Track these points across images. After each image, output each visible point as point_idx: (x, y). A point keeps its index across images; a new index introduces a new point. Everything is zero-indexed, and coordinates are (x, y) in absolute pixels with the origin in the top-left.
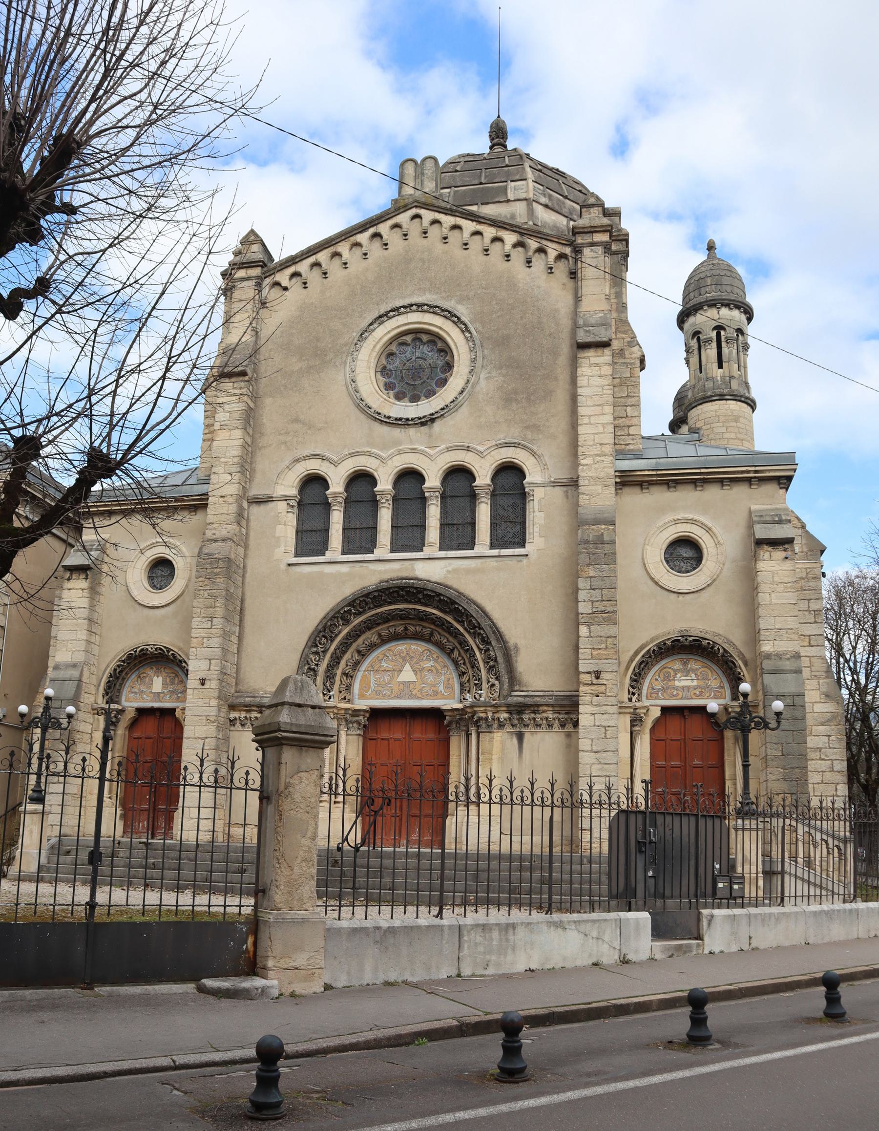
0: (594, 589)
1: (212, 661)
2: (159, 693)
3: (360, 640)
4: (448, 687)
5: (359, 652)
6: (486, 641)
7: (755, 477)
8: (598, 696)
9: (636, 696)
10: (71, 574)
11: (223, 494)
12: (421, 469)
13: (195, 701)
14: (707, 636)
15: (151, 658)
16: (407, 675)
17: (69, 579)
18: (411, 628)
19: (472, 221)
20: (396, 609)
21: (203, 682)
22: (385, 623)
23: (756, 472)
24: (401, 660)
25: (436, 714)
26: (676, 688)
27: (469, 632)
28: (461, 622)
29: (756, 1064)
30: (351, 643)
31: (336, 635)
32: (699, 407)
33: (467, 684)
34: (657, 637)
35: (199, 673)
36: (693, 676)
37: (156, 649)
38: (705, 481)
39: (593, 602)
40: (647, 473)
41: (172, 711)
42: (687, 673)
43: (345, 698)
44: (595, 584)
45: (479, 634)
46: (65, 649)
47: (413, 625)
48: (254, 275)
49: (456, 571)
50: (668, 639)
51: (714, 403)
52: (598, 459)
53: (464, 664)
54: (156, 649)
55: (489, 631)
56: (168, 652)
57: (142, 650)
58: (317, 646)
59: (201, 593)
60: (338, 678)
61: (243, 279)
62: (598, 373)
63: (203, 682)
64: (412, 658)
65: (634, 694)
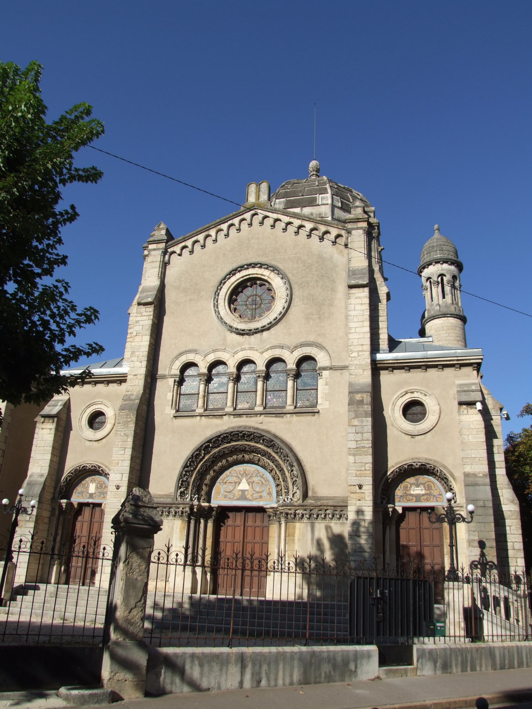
0: (357, 433)
1: (124, 475)
2: (93, 494)
7: (457, 364)
8: (359, 500)
9: (386, 500)
10: (45, 420)
11: (136, 374)
12: (298, 359)
13: (112, 499)
14: (430, 462)
15: (89, 472)
16: (244, 485)
17: (43, 423)
19: (287, 216)
20: (237, 445)
21: (118, 487)
23: (458, 360)
24: (240, 476)
25: (261, 510)
26: (412, 495)
32: (432, 322)
33: (280, 492)
34: (399, 463)
35: (115, 482)
36: (422, 487)
37: (92, 467)
38: (445, 366)
39: (357, 441)
40: (391, 362)
41: (100, 505)
42: (418, 486)
44: (359, 429)
45: (288, 461)
46: (37, 465)
48: (161, 247)
50: (405, 465)
51: (440, 319)
52: (360, 353)
53: (279, 479)
54: (92, 467)
56: (99, 468)
57: (84, 467)
59: (120, 432)
61: (155, 250)
62: (360, 302)
63: (118, 487)
65: (384, 499)
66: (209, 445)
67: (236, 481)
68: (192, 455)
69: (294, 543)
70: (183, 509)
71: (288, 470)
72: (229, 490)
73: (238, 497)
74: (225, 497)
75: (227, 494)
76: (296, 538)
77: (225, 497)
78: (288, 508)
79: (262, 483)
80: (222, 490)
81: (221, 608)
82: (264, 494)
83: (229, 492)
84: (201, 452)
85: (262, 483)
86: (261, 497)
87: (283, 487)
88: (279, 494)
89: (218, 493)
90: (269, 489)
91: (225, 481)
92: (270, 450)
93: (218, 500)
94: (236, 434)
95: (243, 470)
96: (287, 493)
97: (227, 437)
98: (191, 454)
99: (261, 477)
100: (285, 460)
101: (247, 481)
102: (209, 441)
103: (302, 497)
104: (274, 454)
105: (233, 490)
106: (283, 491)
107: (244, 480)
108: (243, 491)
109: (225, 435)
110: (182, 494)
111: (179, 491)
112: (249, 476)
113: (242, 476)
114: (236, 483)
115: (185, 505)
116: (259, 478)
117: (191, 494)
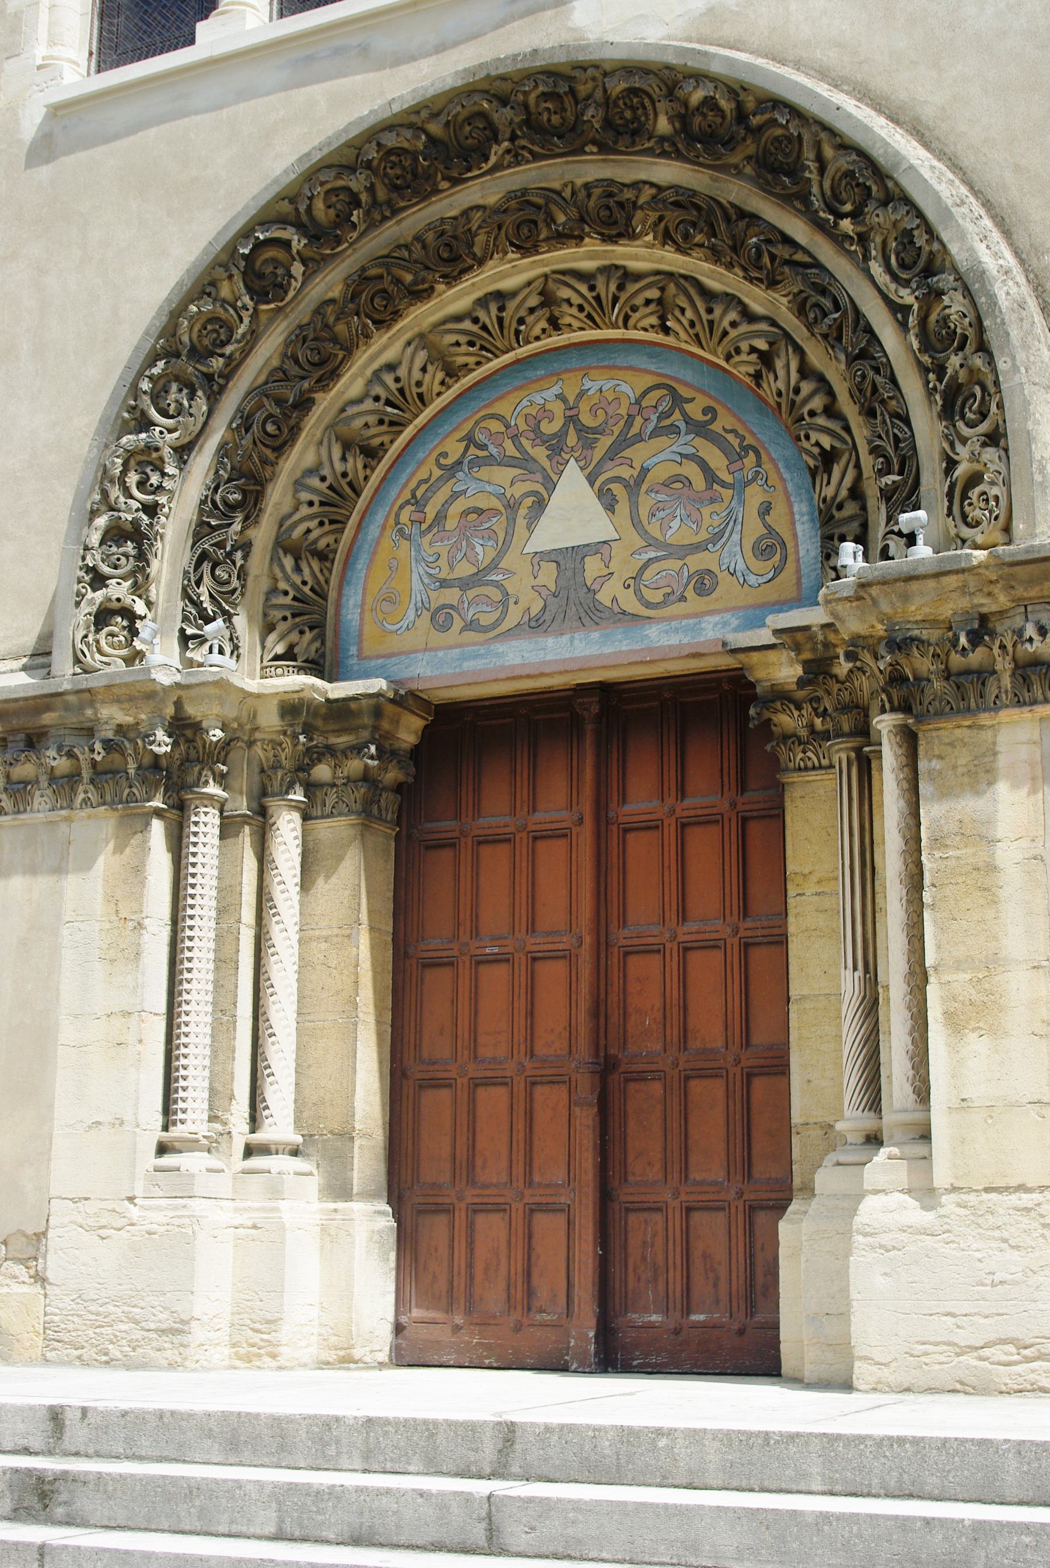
24: (540, 453)
27: (839, 240)
58: (145, 424)
64: (588, 436)
69: (989, 894)
71: (898, 311)
72: (465, 570)
73: (536, 609)
74: (441, 618)
75: (452, 596)
77: (441, 618)
79: (710, 476)
85: (710, 476)
86: (704, 583)
87: (867, 461)
90: (766, 509)
95: (558, 408)
99: (700, 429)
101: (591, 480)
108: (570, 559)
112: (605, 442)
113: (556, 446)
114: (512, 506)
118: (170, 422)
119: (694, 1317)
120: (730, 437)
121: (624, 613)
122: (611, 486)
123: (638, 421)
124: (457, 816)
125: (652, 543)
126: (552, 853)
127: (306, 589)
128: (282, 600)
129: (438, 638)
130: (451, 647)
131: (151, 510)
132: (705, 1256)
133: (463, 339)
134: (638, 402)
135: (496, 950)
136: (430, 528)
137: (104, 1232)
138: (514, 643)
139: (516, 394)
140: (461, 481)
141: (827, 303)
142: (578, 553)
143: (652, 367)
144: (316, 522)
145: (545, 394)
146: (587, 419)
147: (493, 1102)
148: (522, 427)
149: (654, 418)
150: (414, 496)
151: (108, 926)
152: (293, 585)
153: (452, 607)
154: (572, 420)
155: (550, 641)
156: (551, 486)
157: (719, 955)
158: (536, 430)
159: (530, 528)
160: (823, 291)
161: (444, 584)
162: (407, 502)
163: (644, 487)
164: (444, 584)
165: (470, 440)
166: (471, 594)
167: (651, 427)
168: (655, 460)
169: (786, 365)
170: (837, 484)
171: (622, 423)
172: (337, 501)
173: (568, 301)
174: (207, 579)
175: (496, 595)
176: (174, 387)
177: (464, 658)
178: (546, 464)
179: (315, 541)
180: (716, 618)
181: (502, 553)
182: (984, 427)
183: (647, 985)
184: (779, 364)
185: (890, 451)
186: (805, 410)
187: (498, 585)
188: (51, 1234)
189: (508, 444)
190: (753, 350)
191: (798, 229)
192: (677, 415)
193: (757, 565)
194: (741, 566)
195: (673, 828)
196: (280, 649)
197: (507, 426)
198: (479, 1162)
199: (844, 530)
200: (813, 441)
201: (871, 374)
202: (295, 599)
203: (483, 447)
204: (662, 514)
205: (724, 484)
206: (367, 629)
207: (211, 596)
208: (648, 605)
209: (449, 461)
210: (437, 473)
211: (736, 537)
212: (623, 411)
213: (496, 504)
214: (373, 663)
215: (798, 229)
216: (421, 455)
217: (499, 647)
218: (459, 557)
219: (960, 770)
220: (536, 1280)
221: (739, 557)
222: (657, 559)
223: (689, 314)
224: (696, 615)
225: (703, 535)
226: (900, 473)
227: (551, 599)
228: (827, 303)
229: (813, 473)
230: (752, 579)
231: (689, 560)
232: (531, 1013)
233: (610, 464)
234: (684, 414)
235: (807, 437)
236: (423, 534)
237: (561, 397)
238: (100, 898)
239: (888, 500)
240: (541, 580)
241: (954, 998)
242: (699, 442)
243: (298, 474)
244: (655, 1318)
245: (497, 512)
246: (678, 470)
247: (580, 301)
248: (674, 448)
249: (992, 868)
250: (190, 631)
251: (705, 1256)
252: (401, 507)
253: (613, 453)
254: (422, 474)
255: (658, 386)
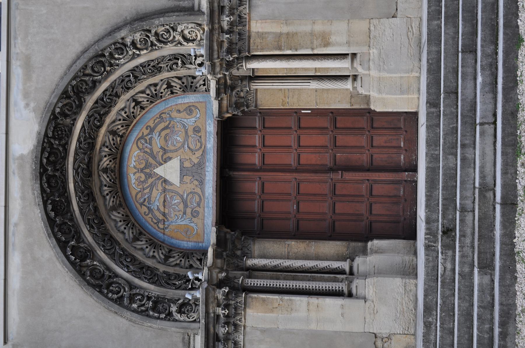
3: (119, 237)
4: (190, 109)
5: (136, 239)
6: (121, 47)
16: (170, 171)
18: (105, 162)
20: (75, 182)
22: (94, 200)
24: (150, 181)
25: (228, 131)
27: (109, 73)
28: (95, 84)
29: (504, 84)
30: (123, 250)
31: (108, 268)
33: (184, 80)
43: (200, 260)
45: (111, 55)
47: (100, 160)
49: (26, 95)
53: (155, 85)
55: (108, 41)
58: (122, 297)
60: (171, 270)
64: (148, 165)
66: (73, 248)
67: (160, 188)
68: (94, 286)
70: (219, 306)
71: (134, 56)
72: (181, 206)
73: (196, 183)
75: (189, 210)
76: (285, 29)
77: (195, 214)
78: (216, 47)
79: (166, 128)
80: (179, 222)
81: (431, 64)
82: (190, 121)
83: (186, 206)
84: (88, 266)
86: (197, 130)
88: (189, 85)
89: (187, 230)
90: (179, 111)
91: (161, 217)
92: (90, 102)
93: (205, 228)
94: (48, 182)
95: (138, 175)
96: (185, 59)
97: (53, 203)
98: (91, 289)
99: (152, 130)
100: (111, 65)
102: (62, 245)
103: (192, 17)
104: (98, 93)
105: (182, 197)
106: (182, 72)
107: (159, 171)
108: (183, 172)
109: (50, 207)
110: (185, 307)
111: (177, 316)
112: (151, 160)
113: (149, 176)
114: (164, 190)
115: (211, 300)
116: (155, 135)
117: (185, 289)
118: (122, 290)
119: (402, 146)
120: (156, 121)
121: (202, 155)
122: (164, 158)
123: (146, 149)
124: (254, 218)
125: (183, 146)
126: (268, 188)
127: (180, 255)
128: (183, 262)
129: (200, 216)
130: (204, 211)
131: (149, 298)
132: (386, 142)
133: (112, 199)
134: (141, 150)
135: (295, 206)
136: (166, 218)
137: (375, 312)
138: (206, 190)
139: (131, 190)
140: (154, 207)
141: (127, 79)
142: (182, 168)
143: (131, 145)
144: (160, 251)
145: (132, 179)
146: (142, 166)
147: (342, 140)
148: (141, 187)
149: (146, 145)
150: (156, 223)
151: (280, 311)
152: (179, 258)
153: (192, 210)
154: (142, 170)
155: (207, 178)
156: (161, 177)
157: (302, 136)
158: (143, 182)
159: (171, 184)
160: (123, 81)
161: (185, 213)
162: (158, 225)
163: (166, 148)
164: (185, 213)
165: (142, 204)
166: (189, 204)
167: (149, 146)
168: (158, 144)
169: (142, 98)
170: (176, 84)
171: (146, 155)
172: (155, 243)
173: (108, 165)
174: (174, 282)
175: (190, 196)
176: (111, 288)
177: (208, 207)
178: (154, 179)
179: (166, 252)
180: (208, 127)
181: (178, 194)
182: (171, 31)
183: (309, 158)
184: (140, 100)
185: (172, 62)
186: (154, 92)
187: (188, 195)
188: (375, 332)
189: (145, 191)
190: (134, 108)
191: (105, 85)
192: (147, 138)
193: (194, 114)
194: (194, 119)
195: (265, 149)
196: (198, 263)
197: (140, 191)
198: (357, 212)
199: (190, 82)
200: (163, 91)
201: (150, 67)
202: (183, 258)
203: (145, 200)
204: (175, 143)
205: (169, 124)
206: (195, 240)
207: (179, 280)
208: (201, 147)
209: (147, 211)
210: (150, 215)
211: (185, 120)
212: (142, 154)
213: (163, 195)
214: (206, 238)
215: (105, 85)
216: (144, 221)
217: (207, 194)
218: (177, 208)
219: (261, 41)
220: (391, 195)
221: (191, 120)
222: (188, 144)
223: (119, 127)
224: (206, 133)
225: (183, 130)
226: (178, 59)
227: (195, 178)
228: (127, 79)
229: (172, 93)
230: (198, 116)
231: (189, 135)
232: (315, 195)
233: (158, 158)
234: (147, 135)
235: (162, 93)
236: (168, 221)
237: (134, 174)
238: (271, 315)
239: (185, 64)
240: (188, 181)
241: (321, 45)
242: (155, 131)
243: (144, 256)
244: (402, 158)
245: (165, 196)
246: (163, 137)
247: (108, 161)
248: (156, 139)
249: (288, 34)
250: (190, 287)
251: (386, 142)
252: (159, 228)
253: (154, 157)
254: (150, 220)
255: (137, 143)
